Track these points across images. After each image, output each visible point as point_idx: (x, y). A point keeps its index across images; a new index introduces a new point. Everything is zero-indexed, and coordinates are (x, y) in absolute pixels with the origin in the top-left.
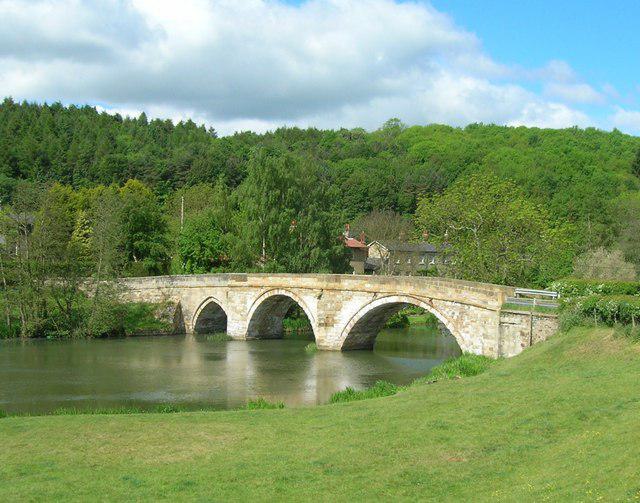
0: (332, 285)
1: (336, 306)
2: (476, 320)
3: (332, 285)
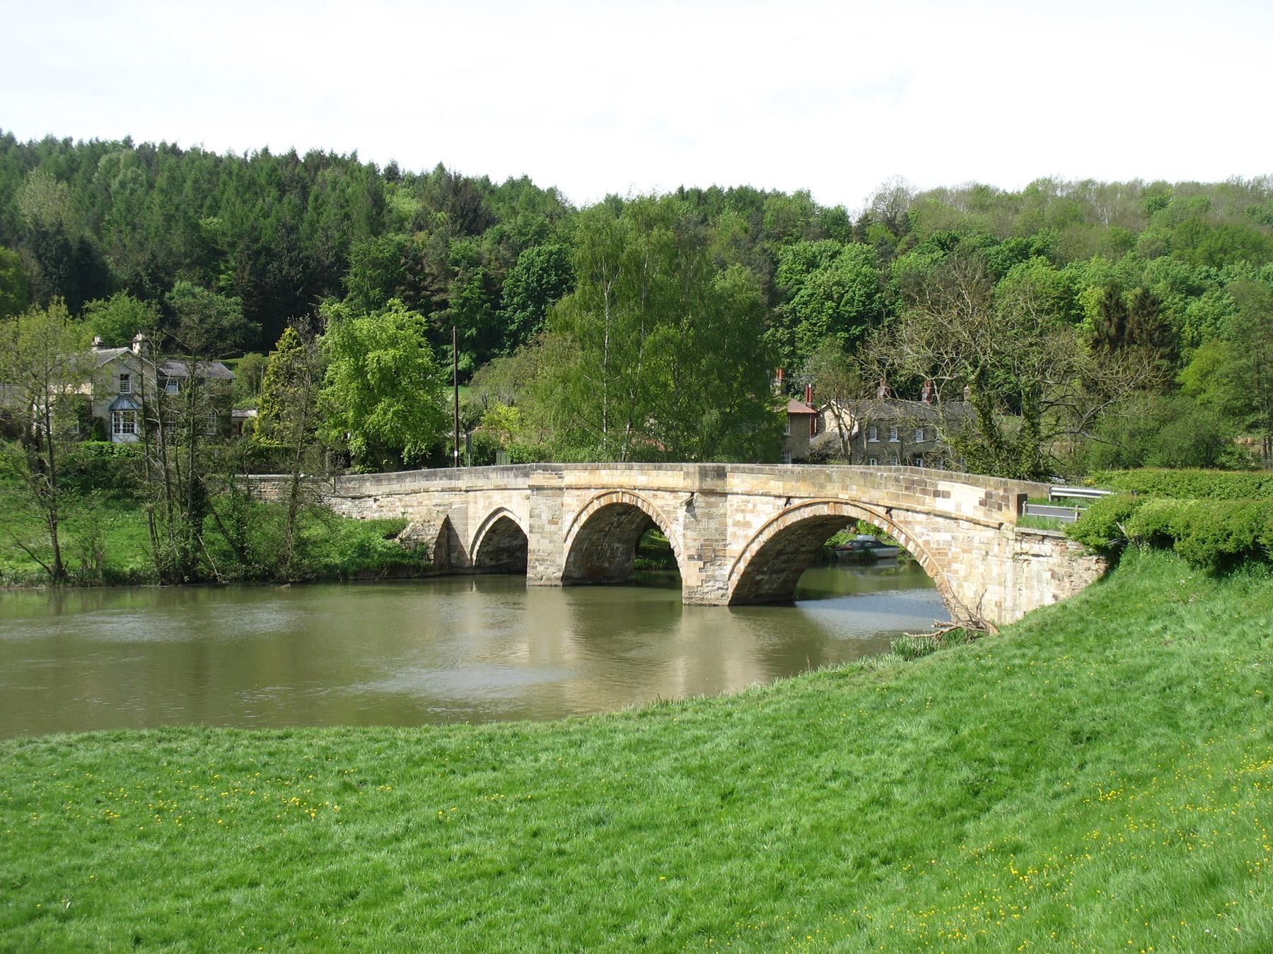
0: (709, 484)
1: (727, 516)
2: (988, 556)
3: (709, 484)
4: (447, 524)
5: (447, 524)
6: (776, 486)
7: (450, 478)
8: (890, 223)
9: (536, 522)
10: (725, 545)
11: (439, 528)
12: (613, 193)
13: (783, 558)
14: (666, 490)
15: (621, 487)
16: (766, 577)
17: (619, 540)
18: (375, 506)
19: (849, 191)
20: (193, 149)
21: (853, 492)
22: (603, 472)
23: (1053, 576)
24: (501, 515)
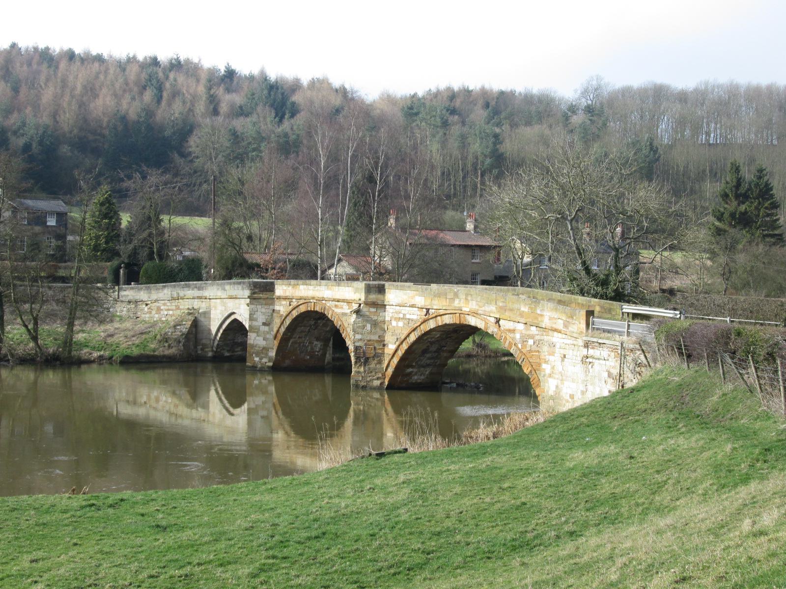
2: (572, 356)
3: (373, 297)
4: (195, 324)
5: (195, 324)
6: (420, 301)
7: (199, 289)
8: (589, 110)
9: (255, 323)
10: (384, 345)
11: (188, 326)
12: (299, 78)
13: (428, 355)
14: (344, 301)
15: (313, 298)
16: (415, 370)
17: (318, 339)
18: (146, 309)
19: (566, 87)
20: (511, 91)
21: (472, 305)
22: (302, 287)
23: (609, 376)
24: (233, 317)
